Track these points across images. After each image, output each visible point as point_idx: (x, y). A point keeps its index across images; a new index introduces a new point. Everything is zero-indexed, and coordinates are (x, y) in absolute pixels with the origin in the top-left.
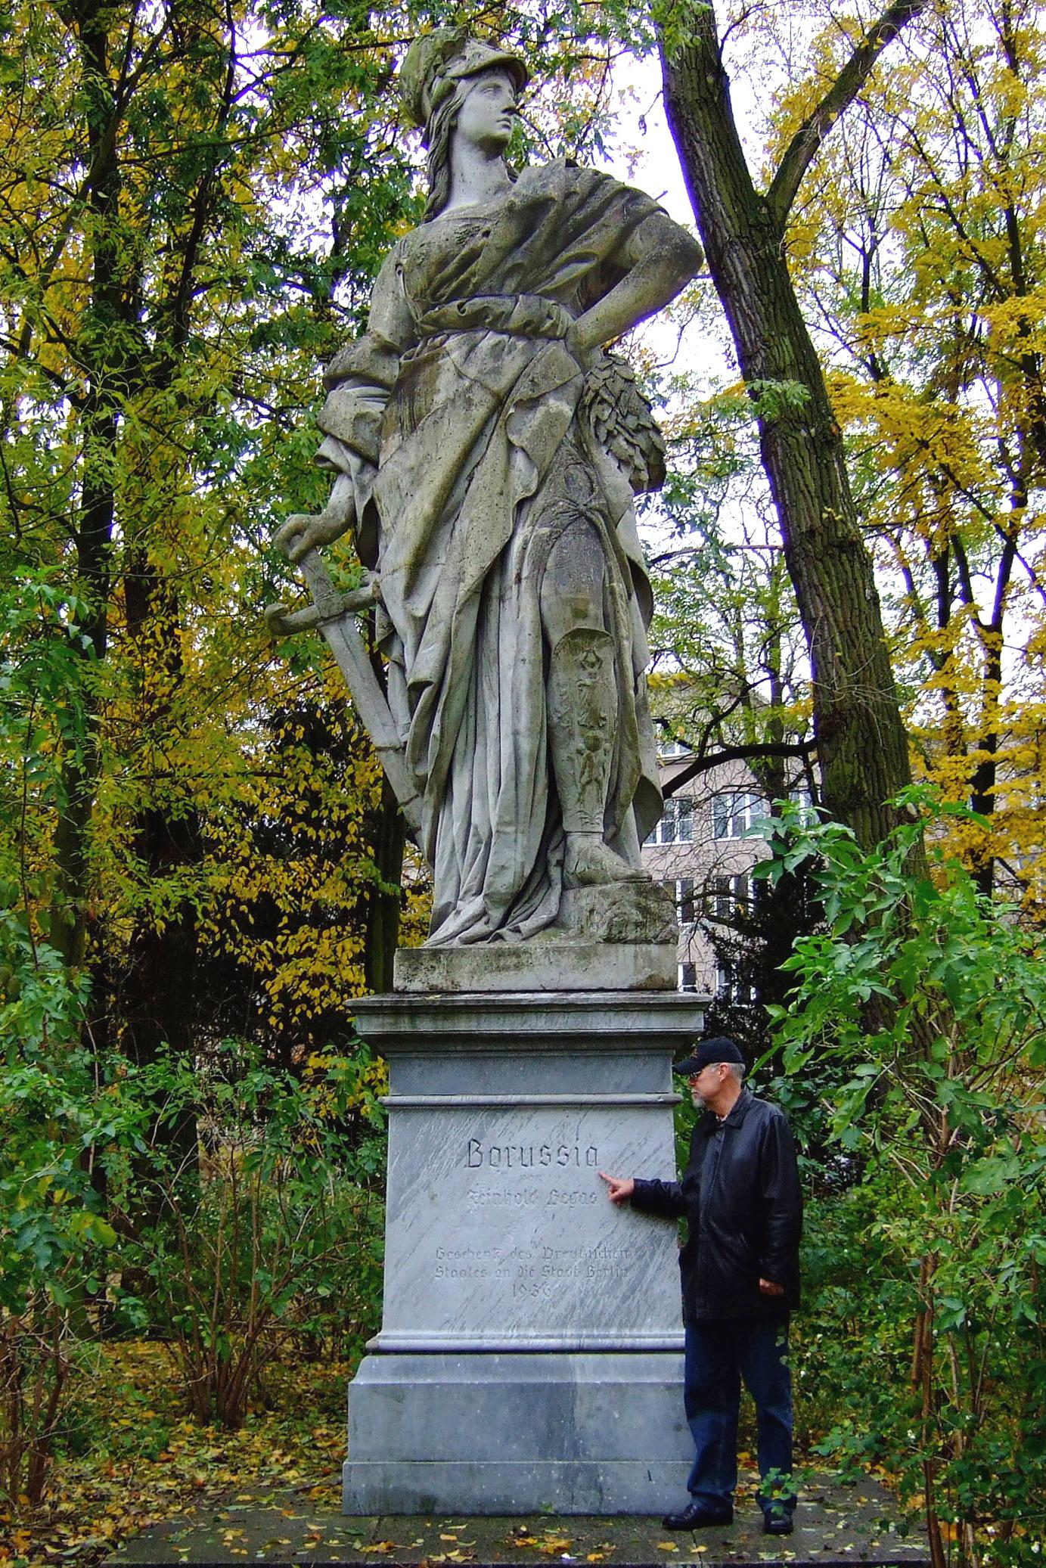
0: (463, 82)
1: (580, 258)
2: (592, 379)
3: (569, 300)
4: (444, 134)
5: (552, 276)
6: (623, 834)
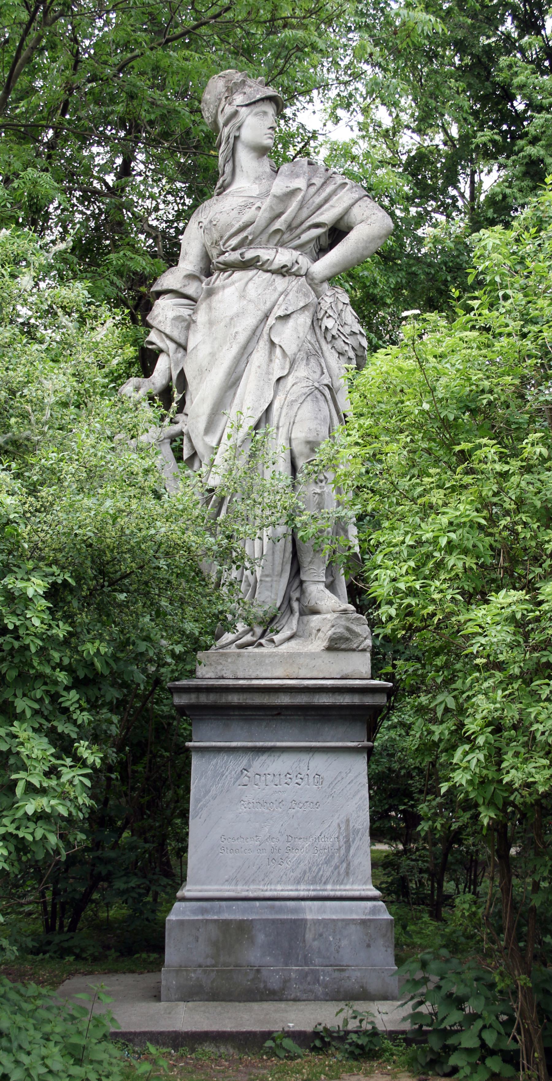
0: (244, 108)
1: (317, 226)
2: (323, 302)
3: (308, 250)
4: (232, 140)
5: (299, 236)
6: (336, 582)
